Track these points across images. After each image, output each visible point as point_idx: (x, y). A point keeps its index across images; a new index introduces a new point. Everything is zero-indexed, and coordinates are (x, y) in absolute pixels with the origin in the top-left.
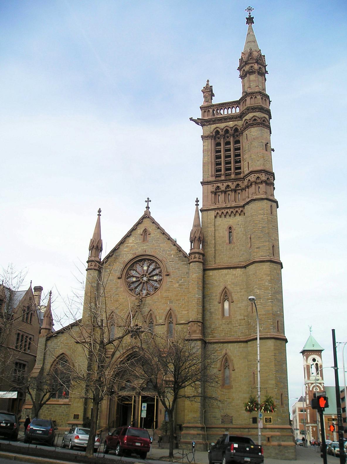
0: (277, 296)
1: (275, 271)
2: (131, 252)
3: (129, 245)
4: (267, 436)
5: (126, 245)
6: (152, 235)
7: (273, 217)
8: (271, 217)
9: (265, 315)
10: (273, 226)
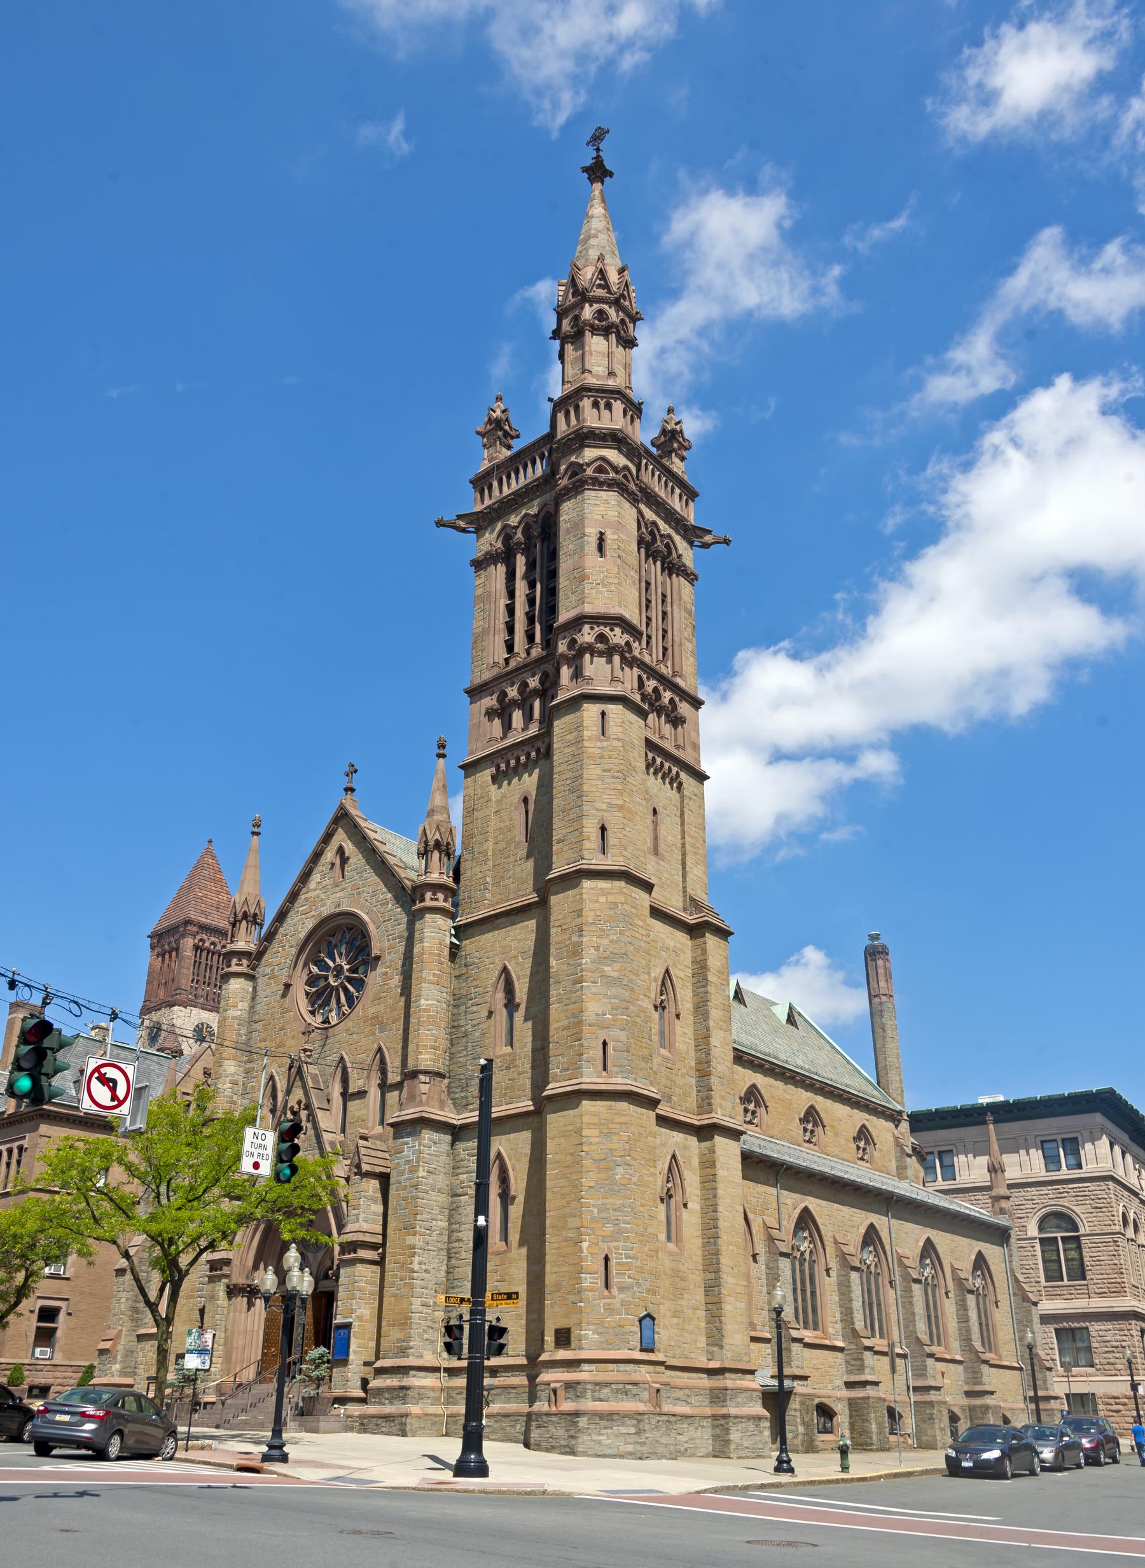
0: (606, 968)
1: (602, 899)
2: (313, 913)
3: (309, 895)
4: (553, 1385)
5: (303, 897)
6: (351, 861)
7: (605, 744)
8: (599, 744)
9: (567, 1028)
10: (604, 771)
